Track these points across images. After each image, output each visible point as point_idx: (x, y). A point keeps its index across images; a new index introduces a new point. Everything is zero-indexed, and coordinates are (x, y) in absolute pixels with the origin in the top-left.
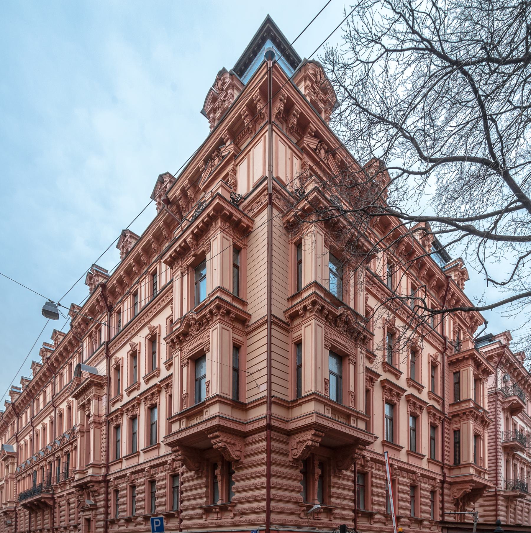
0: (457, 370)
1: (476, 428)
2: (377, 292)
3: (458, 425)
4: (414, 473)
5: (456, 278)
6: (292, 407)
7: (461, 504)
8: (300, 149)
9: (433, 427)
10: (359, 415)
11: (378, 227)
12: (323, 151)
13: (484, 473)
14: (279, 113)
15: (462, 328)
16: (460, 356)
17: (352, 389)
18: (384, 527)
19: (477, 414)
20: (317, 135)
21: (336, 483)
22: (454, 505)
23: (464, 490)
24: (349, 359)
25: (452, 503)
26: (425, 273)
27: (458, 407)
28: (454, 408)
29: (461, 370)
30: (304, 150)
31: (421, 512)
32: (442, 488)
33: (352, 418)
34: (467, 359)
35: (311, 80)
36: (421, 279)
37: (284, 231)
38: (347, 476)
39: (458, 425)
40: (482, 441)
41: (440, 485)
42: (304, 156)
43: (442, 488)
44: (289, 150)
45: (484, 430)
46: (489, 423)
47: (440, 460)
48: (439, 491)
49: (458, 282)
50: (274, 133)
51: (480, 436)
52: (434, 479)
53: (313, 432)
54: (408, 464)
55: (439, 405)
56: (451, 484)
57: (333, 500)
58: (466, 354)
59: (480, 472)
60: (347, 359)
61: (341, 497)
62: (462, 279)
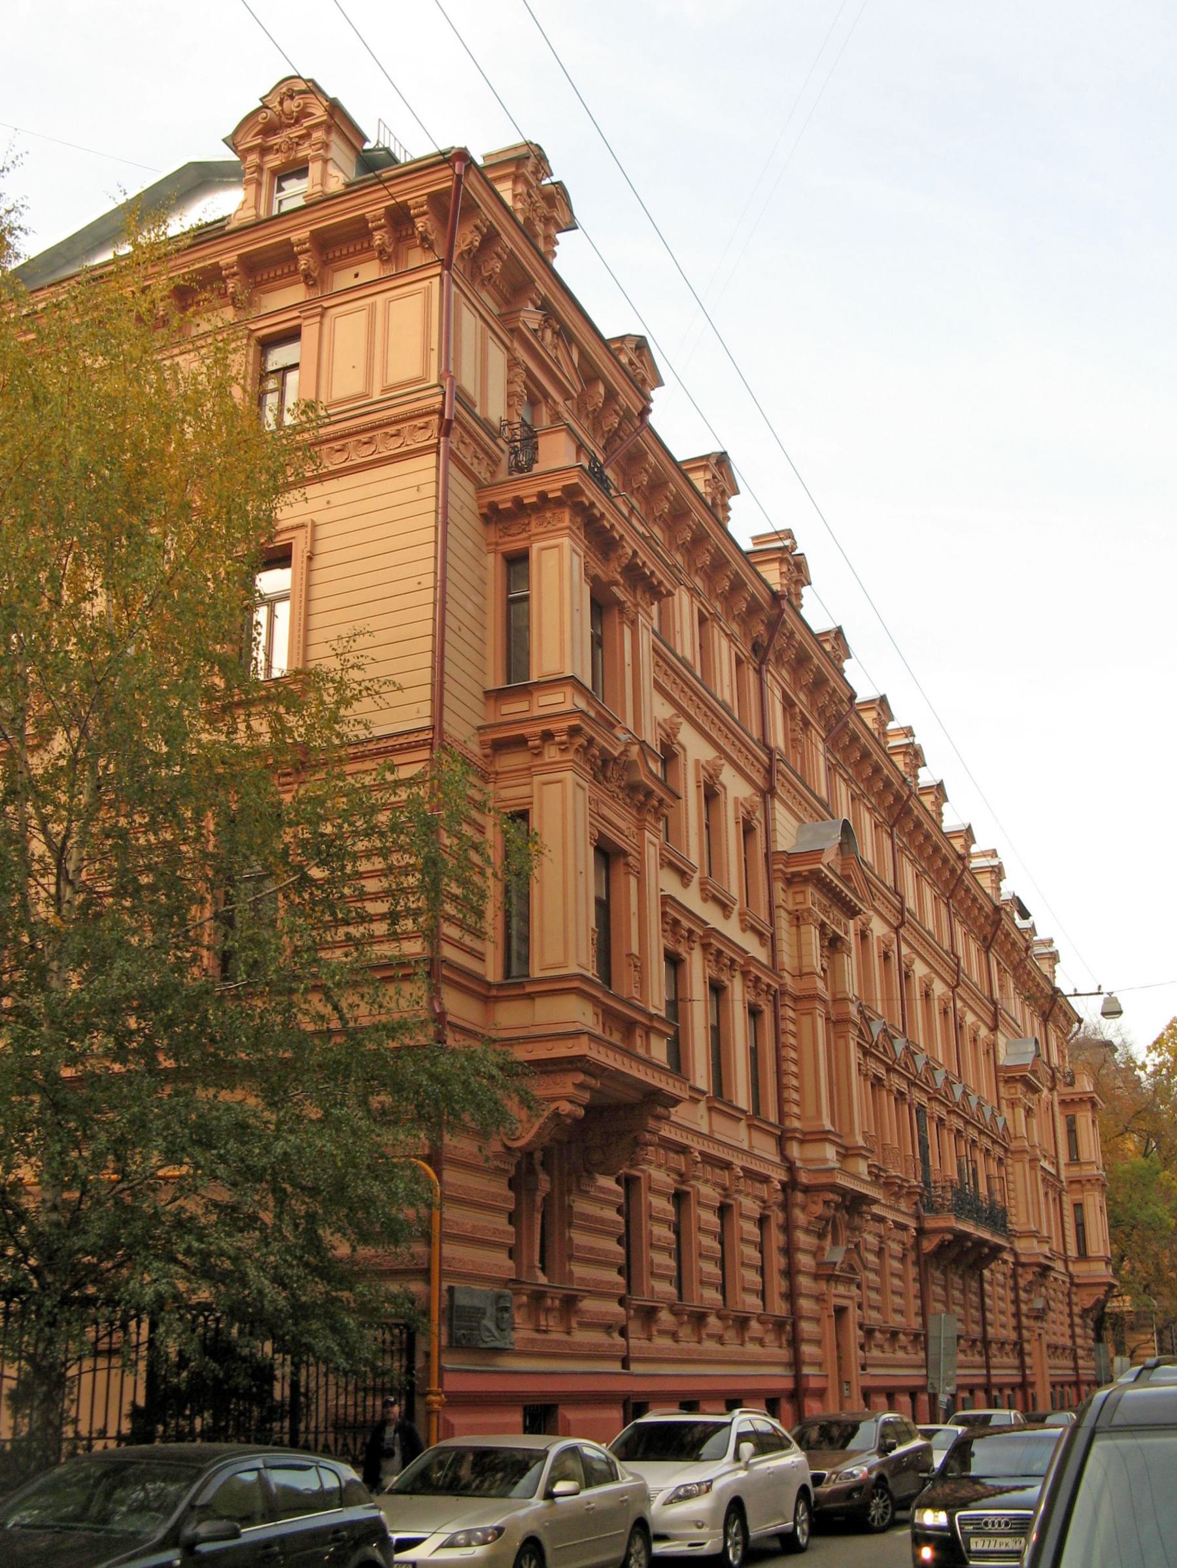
0: (520, 545)
1: (606, 811)
2: (462, 446)
3: (524, 791)
4: (727, 1166)
5: (709, 490)
6: (497, 999)
7: (544, 1183)
8: (506, 325)
9: (754, 1013)
10: (656, 1024)
11: (495, 285)
12: (548, 334)
13: (648, 1030)
14: (469, 251)
15: (546, 395)
16: (528, 492)
17: (635, 950)
18: (718, 1347)
19: (603, 750)
20: (545, 306)
21: (587, 1217)
22: (512, 1185)
23: (553, 1106)
24: (627, 864)
25: (499, 1172)
26: (666, 506)
27: (524, 706)
28: (506, 709)
29: (535, 547)
30: (514, 332)
31: (702, 1283)
32: (785, 1206)
33: (638, 1032)
34: (559, 503)
35: (527, 183)
36: (632, 494)
37: (478, 524)
38: (602, 1189)
39: (524, 791)
40: (633, 882)
41: (780, 1197)
42: (516, 345)
43: (785, 1206)
44: (480, 323)
45: (641, 828)
46: (661, 801)
47: (773, 1118)
48: (777, 1217)
49: (713, 499)
50: (454, 289)
51: (625, 854)
52: (766, 1179)
53: (580, 1078)
54: (709, 1138)
55: (763, 945)
56: (807, 1189)
57: (579, 1270)
58: (554, 488)
59: (629, 1027)
60: (622, 861)
61: (596, 1260)
62: (548, 220)
